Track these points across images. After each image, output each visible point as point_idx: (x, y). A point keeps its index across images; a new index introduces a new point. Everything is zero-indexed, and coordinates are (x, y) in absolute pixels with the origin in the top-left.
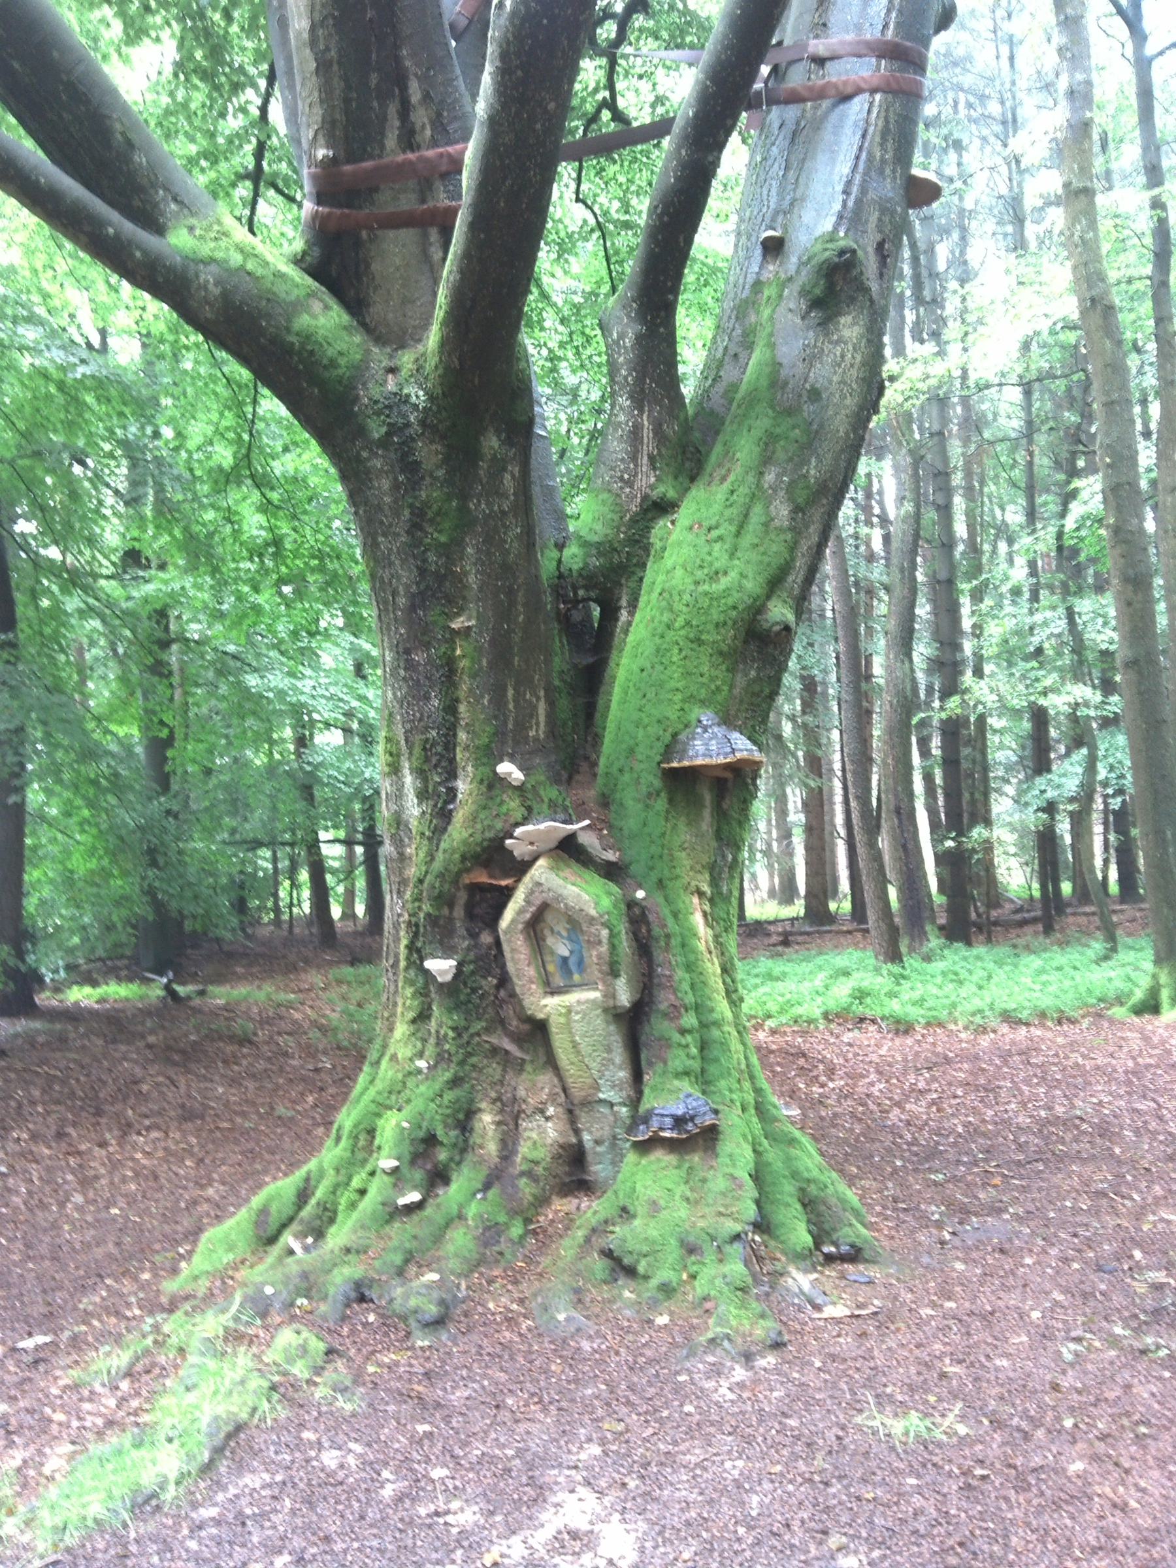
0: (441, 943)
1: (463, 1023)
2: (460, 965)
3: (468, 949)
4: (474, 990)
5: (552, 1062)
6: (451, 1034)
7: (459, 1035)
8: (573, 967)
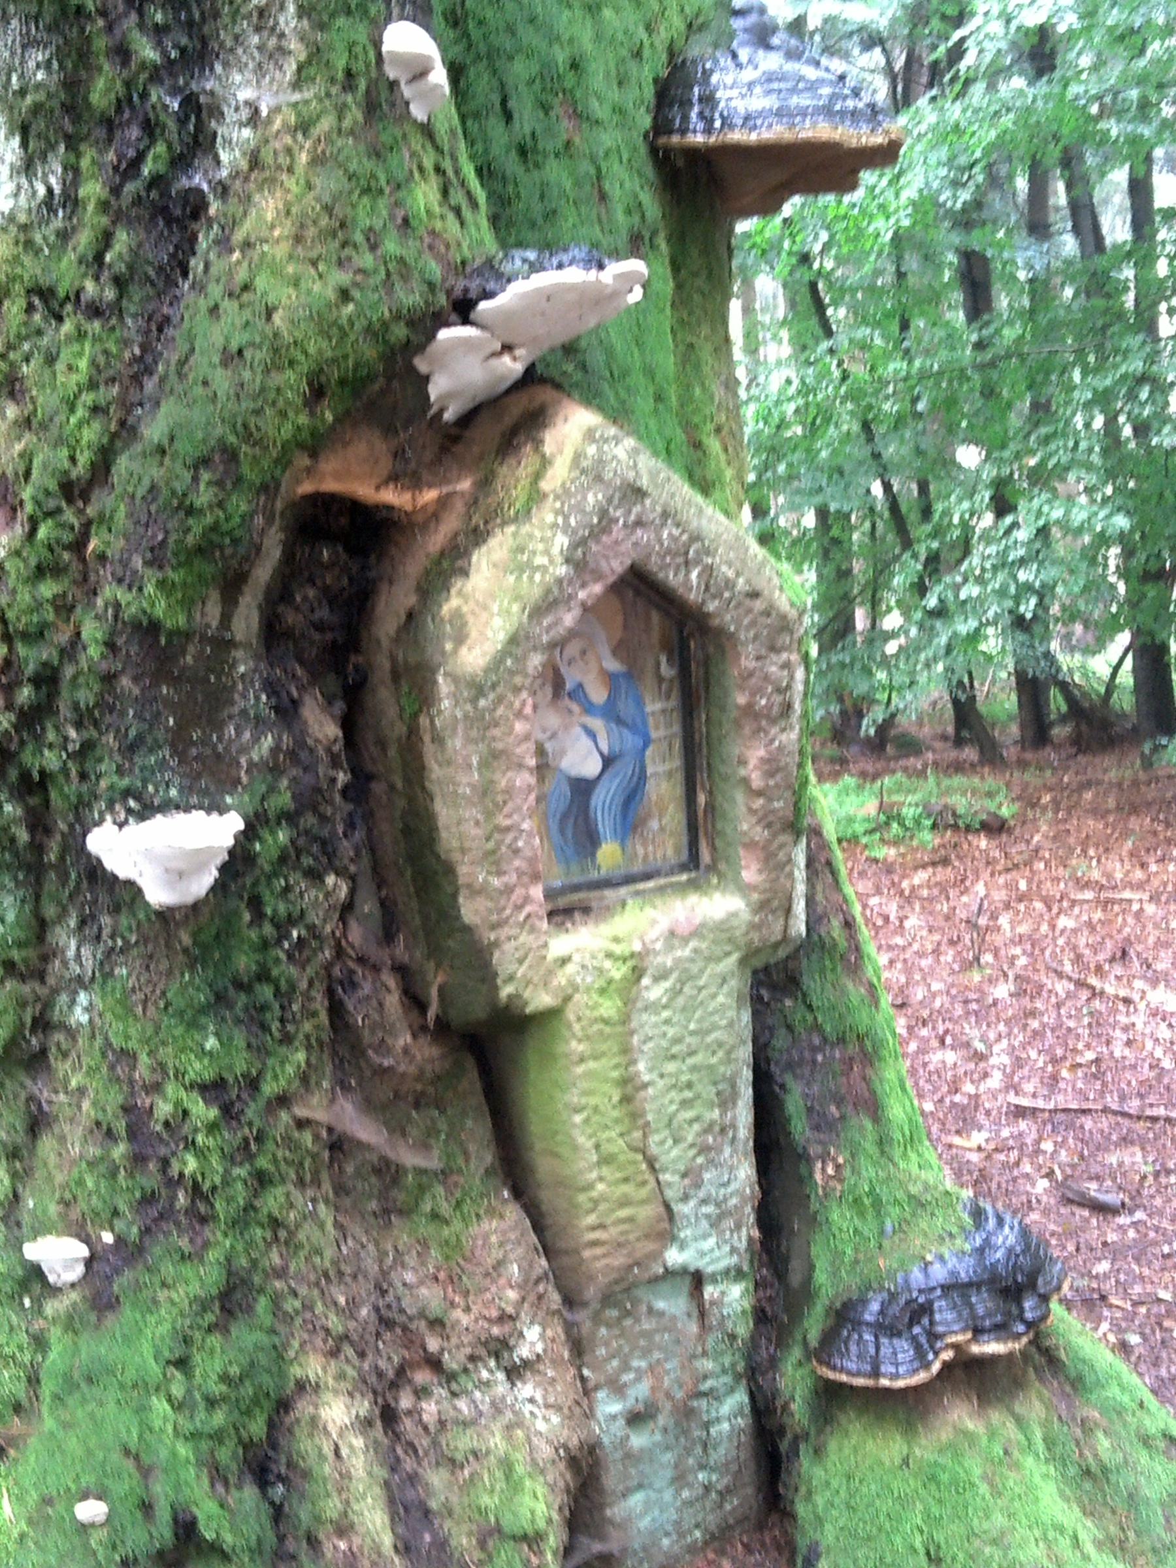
0: (179, 742)
1: (241, 1063)
2: (249, 834)
3: (273, 768)
4: (282, 926)
5: (514, 1170)
6: (202, 1111)
7: (229, 1113)
8: (604, 822)
